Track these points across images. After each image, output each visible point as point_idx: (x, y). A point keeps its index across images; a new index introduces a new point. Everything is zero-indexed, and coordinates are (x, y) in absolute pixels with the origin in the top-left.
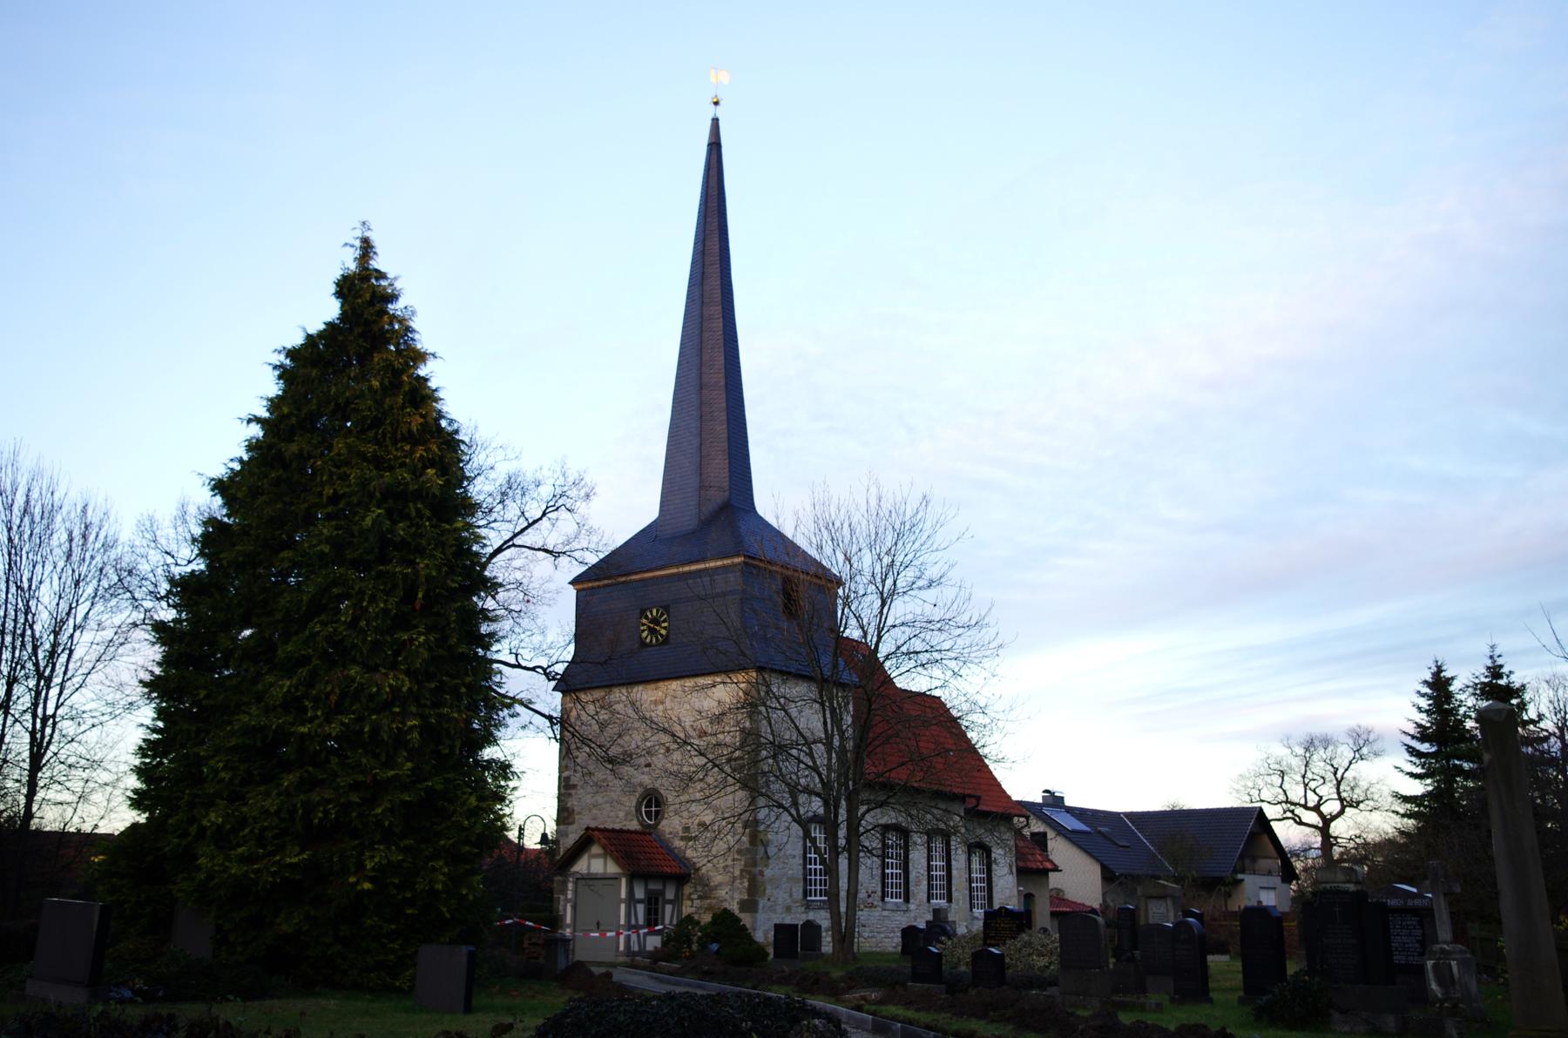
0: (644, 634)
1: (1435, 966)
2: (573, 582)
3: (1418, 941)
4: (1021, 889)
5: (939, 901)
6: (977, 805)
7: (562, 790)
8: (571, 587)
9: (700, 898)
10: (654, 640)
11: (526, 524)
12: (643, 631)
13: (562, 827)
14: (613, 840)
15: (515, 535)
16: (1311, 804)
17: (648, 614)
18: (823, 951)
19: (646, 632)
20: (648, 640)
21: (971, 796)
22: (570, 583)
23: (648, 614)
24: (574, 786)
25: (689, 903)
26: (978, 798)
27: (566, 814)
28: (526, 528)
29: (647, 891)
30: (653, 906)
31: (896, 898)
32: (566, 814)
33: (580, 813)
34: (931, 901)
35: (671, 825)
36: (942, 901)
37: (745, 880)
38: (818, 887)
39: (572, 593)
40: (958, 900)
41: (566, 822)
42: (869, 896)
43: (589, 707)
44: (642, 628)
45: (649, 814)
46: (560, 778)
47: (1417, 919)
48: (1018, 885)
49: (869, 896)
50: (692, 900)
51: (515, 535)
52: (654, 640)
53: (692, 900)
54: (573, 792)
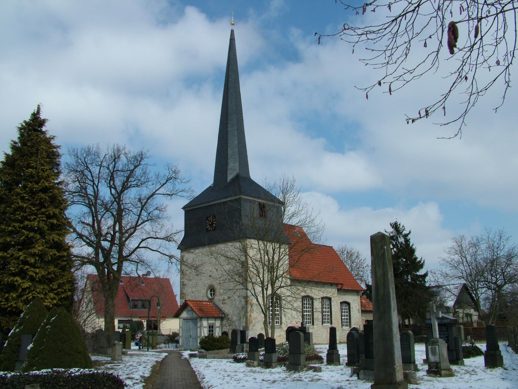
0: (208, 227)
1: (431, 348)
2: (184, 208)
3: (446, 337)
4: (364, 318)
5: (327, 324)
6: (342, 288)
7: (182, 287)
8: (183, 210)
9: (229, 325)
10: (211, 229)
11: (160, 186)
12: (208, 225)
13: (182, 300)
14: (195, 305)
15: (156, 191)
16: (494, 282)
17: (209, 219)
18: (508, 341)
19: (208, 226)
20: (209, 229)
21: (339, 284)
22: (182, 208)
23: (209, 219)
24: (185, 285)
25: (225, 327)
26: (342, 284)
27: (183, 295)
28: (160, 188)
29: (208, 323)
30: (211, 329)
31: (326, 323)
32: (183, 295)
33: (188, 295)
34: (324, 324)
35: (218, 298)
36: (328, 324)
37: (244, 318)
38: (327, 320)
39: (183, 212)
40: (335, 323)
41: (183, 298)
42: (297, 323)
43: (190, 256)
44: (207, 224)
45: (211, 294)
46: (180, 282)
47: (446, 327)
48: (362, 317)
49: (297, 323)
50: (226, 326)
51: (156, 191)
52: (211, 229)
53: (226, 326)
54: (185, 287)
